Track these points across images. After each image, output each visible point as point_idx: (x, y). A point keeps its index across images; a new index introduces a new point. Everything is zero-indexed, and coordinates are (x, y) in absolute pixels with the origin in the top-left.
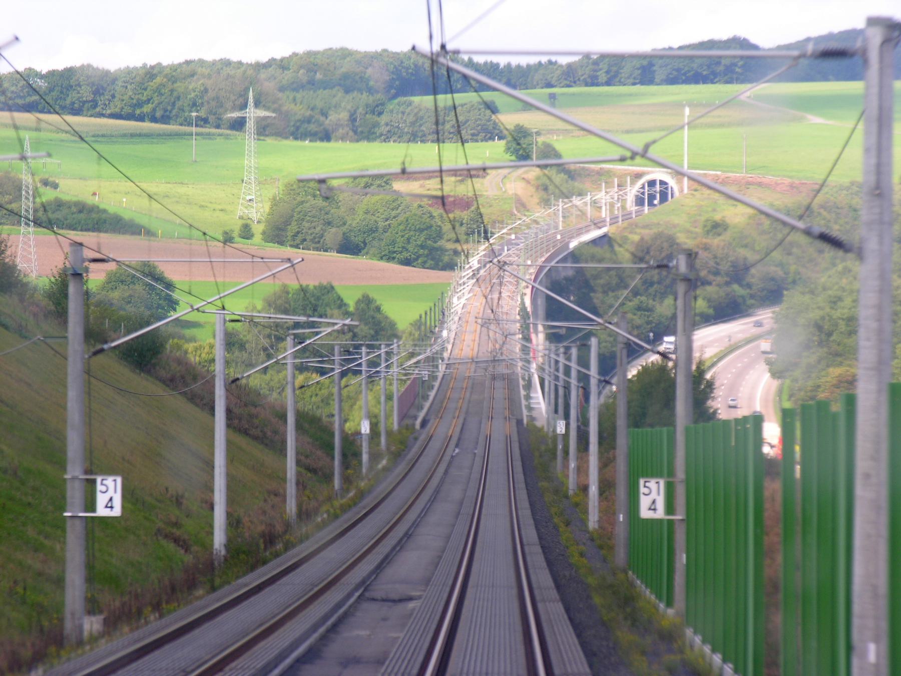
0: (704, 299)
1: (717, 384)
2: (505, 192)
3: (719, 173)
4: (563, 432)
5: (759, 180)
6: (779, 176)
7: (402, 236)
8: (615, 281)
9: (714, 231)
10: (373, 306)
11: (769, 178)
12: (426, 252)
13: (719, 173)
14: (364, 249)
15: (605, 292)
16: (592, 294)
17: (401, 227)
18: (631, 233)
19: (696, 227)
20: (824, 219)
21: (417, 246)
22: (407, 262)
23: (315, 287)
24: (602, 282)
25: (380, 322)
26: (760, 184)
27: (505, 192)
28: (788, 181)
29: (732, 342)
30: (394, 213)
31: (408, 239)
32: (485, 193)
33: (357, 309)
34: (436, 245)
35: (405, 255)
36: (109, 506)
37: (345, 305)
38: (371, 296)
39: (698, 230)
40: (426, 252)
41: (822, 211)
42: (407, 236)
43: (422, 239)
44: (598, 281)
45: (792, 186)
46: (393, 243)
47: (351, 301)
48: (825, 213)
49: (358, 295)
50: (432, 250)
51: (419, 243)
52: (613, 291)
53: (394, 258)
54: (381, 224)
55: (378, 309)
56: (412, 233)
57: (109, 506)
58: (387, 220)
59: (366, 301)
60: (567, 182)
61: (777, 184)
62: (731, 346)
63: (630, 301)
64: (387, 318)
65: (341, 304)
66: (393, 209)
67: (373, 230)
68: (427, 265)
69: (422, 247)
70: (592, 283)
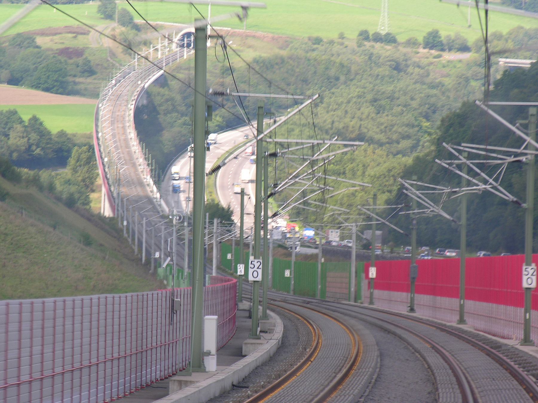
0: (220, 116)
1: (234, 212)
2: (102, 45)
3: (229, 29)
4: (243, 273)
5: (253, 34)
6: (265, 32)
7: (45, 75)
8: (171, 108)
9: (227, 72)
10: (38, 122)
11: (260, 33)
12: (59, 84)
13: (229, 29)
14: (21, 81)
15: (165, 114)
16: (159, 116)
17: (44, 70)
18: (177, 72)
19: (216, 70)
20: (291, 65)
21: (53, 80)
22: (47, 90)
23: (7, 112)
24: (163, 108)
25: (42, 131)
26: (254, 37)
27: (102, 45)
28: (271, 35)
29: (236, 144)
30: (39, 60)
31: (48, 76)
32: (90, 46)
33: (29, 124)
34: (64, 79)
35: (46, 85)
36: (241, 271)
37: (23, 121)
38: (37, 116)
39: (218, 71)
40: (59, 84)
41: (289, 60)
42: (47, 74)
43: (57, 76)
44: (161, 108)
45: (273, 39)
46: (39, 78)
47: (26, 118)
48: (291, 62)
49: (30, 116)
50: (62, 82)
51: (55, 79)
52: (170, 113)
53: (39, 87)
54: (32, 67)
55: (41, 124)
56: (50, 73)
57: (241, 271)
58: (35, 64)
59: (35, 119)
60: (137, 35)
61: (264, 37)
62: (235, 146)
63: (179, 119)
64: (46, 129)
65: (21, 121)
66: (38, 58)
67: (26, 71)
68: (59, 91)
69: (56, 81)
70: (158, 108)
